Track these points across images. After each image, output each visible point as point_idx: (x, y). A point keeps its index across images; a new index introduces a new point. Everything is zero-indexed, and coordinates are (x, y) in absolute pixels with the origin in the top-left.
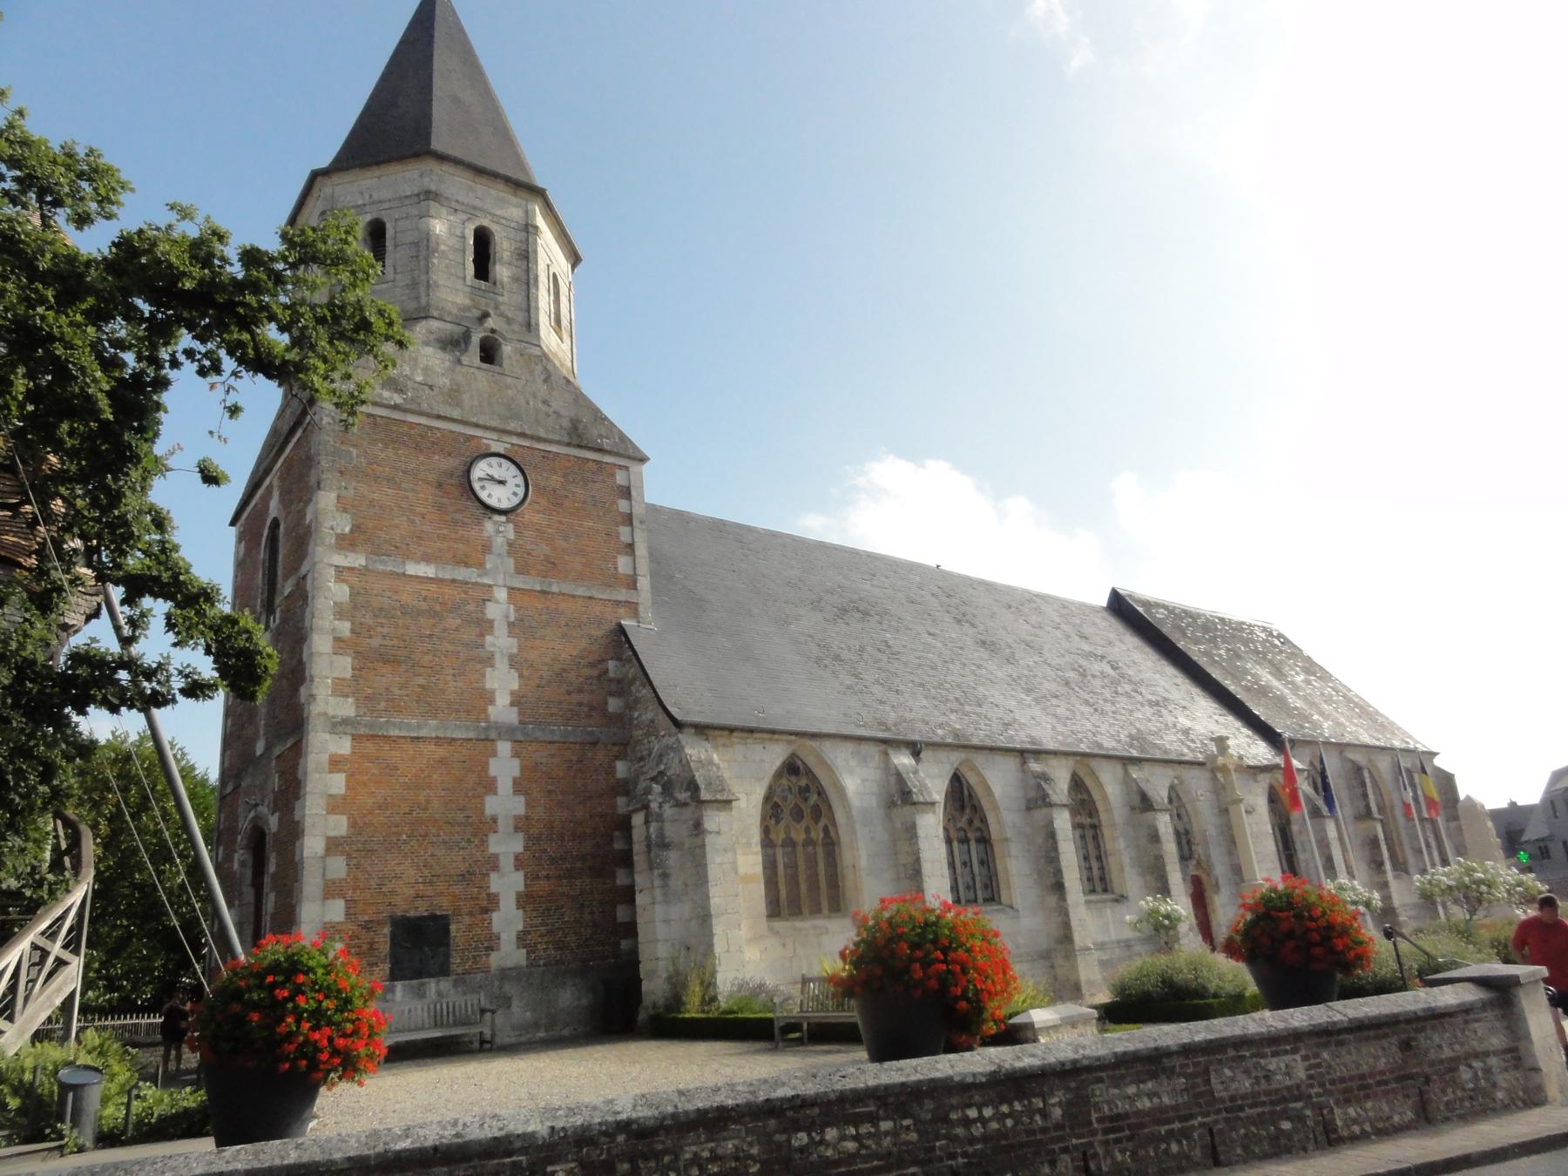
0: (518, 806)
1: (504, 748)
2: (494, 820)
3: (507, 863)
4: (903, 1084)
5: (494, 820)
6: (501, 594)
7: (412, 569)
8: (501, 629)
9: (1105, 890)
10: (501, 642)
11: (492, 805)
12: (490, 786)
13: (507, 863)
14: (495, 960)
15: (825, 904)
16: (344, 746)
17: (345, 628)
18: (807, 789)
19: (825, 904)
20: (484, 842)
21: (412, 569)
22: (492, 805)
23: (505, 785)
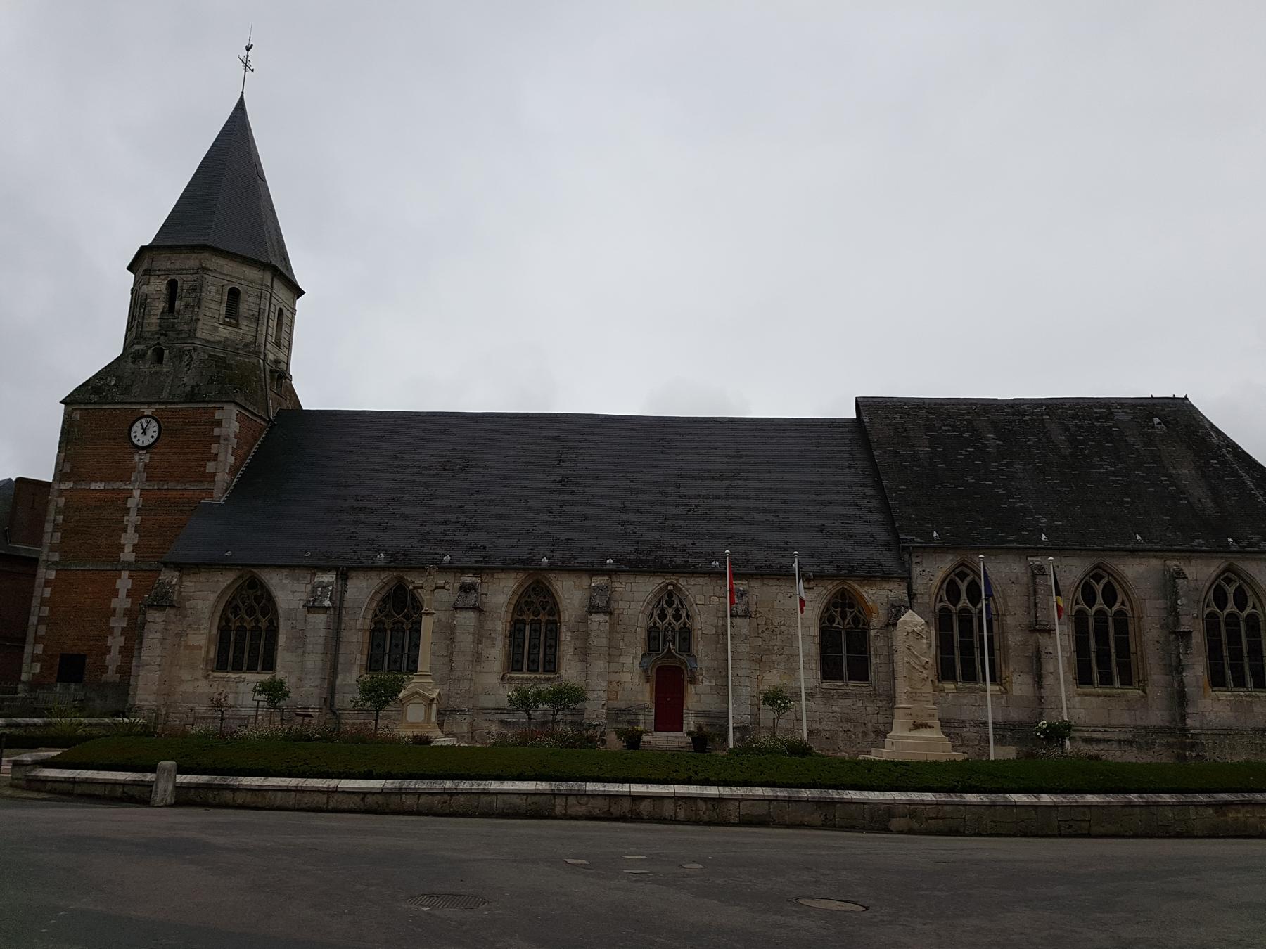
0: (128, 604)
1: (125, 574)
2: (115, 610)
3: (117, 632)
4: (1150, 764)
5: (115, 610)
6: (137, 493)
7: (101, 486)
8: (133, 512)
9: (1127, 681)
10: (133, 518)
11: (115, 603)
12: (115, 593)
13: (117, 632)
14: (104, 678)
15: (1116, 678)
16: (52, 575)
17: (60, 518)
18: (262, 596)
19: (1116, 678)
20: (108, 621)
21: (101, 486)
22: (115, 603)
23: (122, 593)
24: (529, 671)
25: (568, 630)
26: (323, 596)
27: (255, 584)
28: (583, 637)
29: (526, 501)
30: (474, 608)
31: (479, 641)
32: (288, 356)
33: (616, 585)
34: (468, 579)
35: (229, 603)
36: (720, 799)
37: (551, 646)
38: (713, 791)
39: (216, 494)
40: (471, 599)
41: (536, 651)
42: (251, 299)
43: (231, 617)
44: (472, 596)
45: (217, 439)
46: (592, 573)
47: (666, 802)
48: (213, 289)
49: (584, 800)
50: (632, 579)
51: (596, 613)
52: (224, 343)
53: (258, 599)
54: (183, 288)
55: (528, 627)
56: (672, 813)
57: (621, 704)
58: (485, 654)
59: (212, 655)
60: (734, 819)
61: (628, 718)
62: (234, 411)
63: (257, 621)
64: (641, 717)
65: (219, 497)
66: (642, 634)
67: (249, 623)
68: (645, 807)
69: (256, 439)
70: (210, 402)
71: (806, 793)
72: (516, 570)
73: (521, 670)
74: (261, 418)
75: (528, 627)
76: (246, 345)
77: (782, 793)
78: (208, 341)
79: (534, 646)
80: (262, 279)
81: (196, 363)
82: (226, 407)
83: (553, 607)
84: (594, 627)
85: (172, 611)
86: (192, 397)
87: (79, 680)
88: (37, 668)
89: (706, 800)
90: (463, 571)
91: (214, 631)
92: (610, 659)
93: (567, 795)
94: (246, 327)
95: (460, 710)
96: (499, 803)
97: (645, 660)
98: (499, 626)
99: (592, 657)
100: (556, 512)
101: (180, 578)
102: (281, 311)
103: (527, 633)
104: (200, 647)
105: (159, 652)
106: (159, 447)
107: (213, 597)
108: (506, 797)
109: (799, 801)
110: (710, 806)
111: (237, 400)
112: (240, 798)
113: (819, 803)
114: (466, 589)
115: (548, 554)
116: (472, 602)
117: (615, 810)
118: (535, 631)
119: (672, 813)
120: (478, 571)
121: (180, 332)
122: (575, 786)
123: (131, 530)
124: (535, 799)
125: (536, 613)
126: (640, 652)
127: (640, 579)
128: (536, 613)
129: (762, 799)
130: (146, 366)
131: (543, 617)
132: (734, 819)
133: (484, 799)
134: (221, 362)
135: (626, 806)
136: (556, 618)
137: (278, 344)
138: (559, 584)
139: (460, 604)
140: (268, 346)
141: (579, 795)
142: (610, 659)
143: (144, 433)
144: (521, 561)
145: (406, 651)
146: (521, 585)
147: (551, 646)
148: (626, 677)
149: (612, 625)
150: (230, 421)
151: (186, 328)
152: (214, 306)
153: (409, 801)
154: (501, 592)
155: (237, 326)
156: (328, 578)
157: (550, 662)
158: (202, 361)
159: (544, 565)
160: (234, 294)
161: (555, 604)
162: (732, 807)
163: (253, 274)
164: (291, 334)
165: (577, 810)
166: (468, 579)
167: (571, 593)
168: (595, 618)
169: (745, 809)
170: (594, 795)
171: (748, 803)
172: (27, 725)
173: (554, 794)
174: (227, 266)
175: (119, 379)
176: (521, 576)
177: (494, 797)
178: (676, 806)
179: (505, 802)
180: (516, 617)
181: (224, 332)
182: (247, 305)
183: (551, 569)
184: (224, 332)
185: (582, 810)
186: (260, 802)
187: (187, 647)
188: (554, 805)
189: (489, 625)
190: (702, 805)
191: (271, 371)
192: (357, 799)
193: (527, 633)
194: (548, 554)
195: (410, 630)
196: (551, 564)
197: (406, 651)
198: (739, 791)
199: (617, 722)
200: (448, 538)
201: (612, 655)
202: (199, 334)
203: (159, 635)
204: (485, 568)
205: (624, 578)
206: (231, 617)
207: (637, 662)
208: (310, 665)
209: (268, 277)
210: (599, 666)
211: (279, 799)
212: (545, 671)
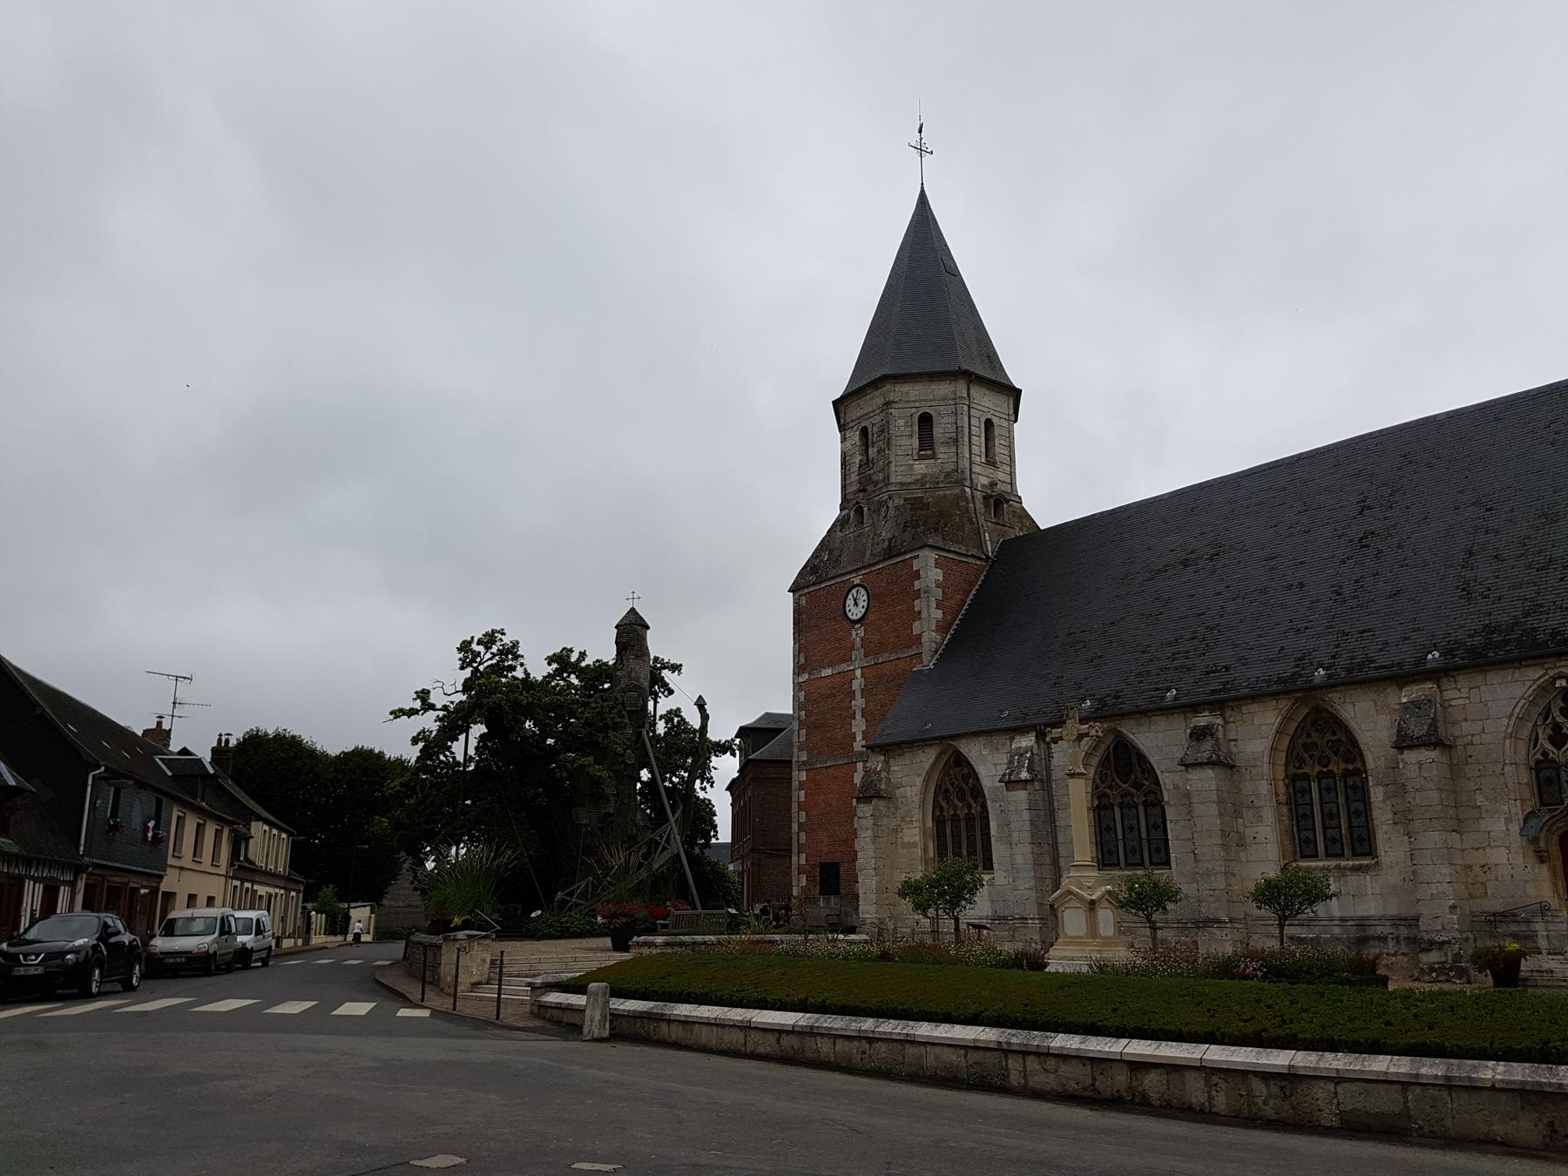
6: (858, 673)
10: (859, 702)
24: (1328, 855)
25: (1378, 784)
26: (1020, 766)
27: (960, 761)
28: (1399, 790)
29: (1301, 585)
30: (1210, 763)
31: (1238, 814)
32: (1012, 474)
33: (1450, 694)
34: (1202, 720)
35: (938, 787)
36: (1290, 1078)
37: (1358, 813)
38: (1280, 1059)
39: (925, 658)
40: (1205, 750)
41: (1334, 823)
42: (946, 419)
43: (944, 804)
44: (1208, 745)
45: (917, 595)
46: (1402, 677)
47: (1191, 1077)
48: (901, 422)
49: (1051, 1063)
50: (1479, 679)
51: (1411, 747)
52: (921, 481)
53: (965, 779)
54: (873, 431)
55: (1314, 786)
56: (1203, 1098)
57: (1497, 905)
58: (1249, 833)
59: (931, 854)
60: (1328, 1119)
61: (1514, 928)
62: (929, 556)
63: (969, 807)
64: (1539, 927)
65: (929, 661)
66: (1518, 777)
67: (962, 813)
68: (1152, 1083)
69: (972, 584)
70: (905, 553)
71: (1493, 1072)
72: (1274, 695)
73: (1315, 856)
74: (973, 556)
75: (1314, 786)
76: (948, 475)
77: (1431, 1068)
78: (902, 484)
79: (1329, 816)
80: (954, 392)
81: (892, 512)
82: (921, 553)
83: (1351, 749)
84: (1412, 772)
85: (882, 803)
86: (890, 553)
87: (837, 892)
88: (804, 882)
89: (1267, 1076)
90: (1194, 708)
91: (929, 824)
92: (1459, 826)
93: (1024, 1053)
94: (944, 453)
95: (1218, 921)
96: (930, 1058)
97: (1533, 822)
98: (1264, 788)
99: (1417, 825)
100: (1347, 592)
101: (886, 762)
102: (989, 424)
103: (1315, 795)
104: (914, 845)
105: (871, 853)
106: (871, 617)
107: (919, 781)
108: (937, 1050)
109: (1474, 1088)
110: (1275, 1089)
111: (931, 542)
112: (676, 1032)
113: (1526, 1095)
114: (1198, 735)
115: (1326, 662)
116: (1206, 755)
117: (1105, 1085)
118: (1328, 789)
119: (1203, 1098)
120: (1219, 704)
121: (876, 483)
122: (1036, 1039)
123: (858, 715)
124: (975, 1057)
125: (1324, 762)
126: (1517, 810)
127: (1494, 678)
128: (1324, 762)
129: (1385, 1081)
130: (850, 532)
131: (1337, 767)
132: (1328, 1119)
133: (910, 1050)
134: (916, 504)
135: (1120, 1080)
136: (1359, 765)
137: (991, 462)
138: (1349, 707)
139: (1189, 760)
140: (976, 469)
141: (1043, 1054)
142: (1459, 826)
143: (856, 604)
144: (1280, 681)
145: (1144, 835)
146: (1286, 719)
147: (1358, 813)
148: (1498, 856)
149: (1455, 771)
150: (929, 569)
151: (881, 476)
152: (906, 440)
153: (825, 1048)
154: (1258, 734)
155: (933, 457)
156: (1027, 741)
157: (1361, 840)
158: (897, 508)
159: (1317, 681)
160: (926, 421)
161: (1354, 742)
162: (1321, 1092)
163: (943, 389)
164: (1011, 447)
165: (1038, 1080)
166: (1202, 720)
167: (1370, 720)
168: (1411, 757)
169: (1350, 1098)
170: (1063, 1057)
171: (1355, 1087)
172: (694, 943)
173: (1004, 1051)
174: (914, 391)
175: (831, 552)
176: (1285, 704)
177: (922, 1049)
178: (1208, 1084)
179: (937, 1058)
180: (1292, 770)
181: (921, 468)
182: (940, 431)
183: (1331, 684)
184: (921, 468)
185: (1050, 1082)
186: (687, 1040)
187: (904, 845)
188: (1007, 1069)
189: (1248, 787)
190: (1259, 1087)
191: (985, 498)
192: (772, 1039)
193: (1315, 795)
194: (1326, 662)
195: (1145, 804)
196: (1329, 676)
197: (1144, 835)
198: (1336, 1062)
199: (1492, 936)
200: (1176, 663)
201: (1460, 816)
202: (893, 480)
203: (869, 833)
204: (1226, 701)
205: (1463, 681)
206: (944, 804)
207: (1515, 828)
208: (1019, 859)
209: (961, 387)
210: (1433, 838)
211: (705, 1036)
212: (1355, 854)
